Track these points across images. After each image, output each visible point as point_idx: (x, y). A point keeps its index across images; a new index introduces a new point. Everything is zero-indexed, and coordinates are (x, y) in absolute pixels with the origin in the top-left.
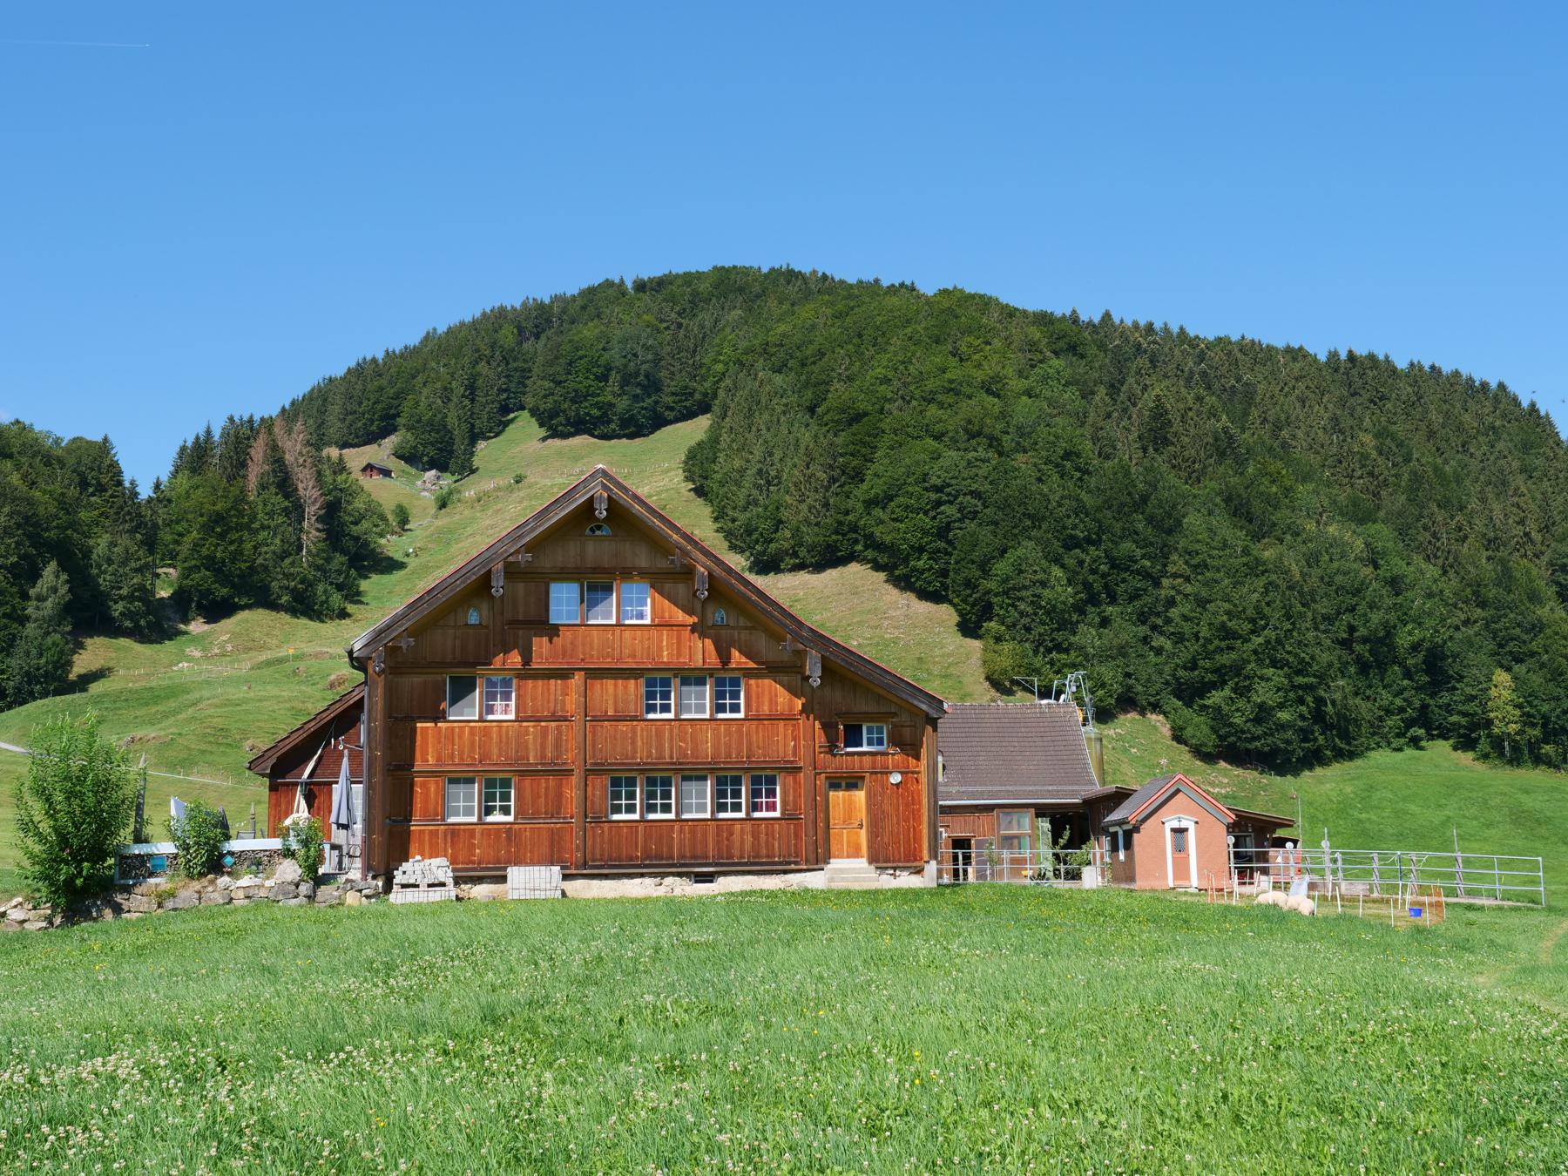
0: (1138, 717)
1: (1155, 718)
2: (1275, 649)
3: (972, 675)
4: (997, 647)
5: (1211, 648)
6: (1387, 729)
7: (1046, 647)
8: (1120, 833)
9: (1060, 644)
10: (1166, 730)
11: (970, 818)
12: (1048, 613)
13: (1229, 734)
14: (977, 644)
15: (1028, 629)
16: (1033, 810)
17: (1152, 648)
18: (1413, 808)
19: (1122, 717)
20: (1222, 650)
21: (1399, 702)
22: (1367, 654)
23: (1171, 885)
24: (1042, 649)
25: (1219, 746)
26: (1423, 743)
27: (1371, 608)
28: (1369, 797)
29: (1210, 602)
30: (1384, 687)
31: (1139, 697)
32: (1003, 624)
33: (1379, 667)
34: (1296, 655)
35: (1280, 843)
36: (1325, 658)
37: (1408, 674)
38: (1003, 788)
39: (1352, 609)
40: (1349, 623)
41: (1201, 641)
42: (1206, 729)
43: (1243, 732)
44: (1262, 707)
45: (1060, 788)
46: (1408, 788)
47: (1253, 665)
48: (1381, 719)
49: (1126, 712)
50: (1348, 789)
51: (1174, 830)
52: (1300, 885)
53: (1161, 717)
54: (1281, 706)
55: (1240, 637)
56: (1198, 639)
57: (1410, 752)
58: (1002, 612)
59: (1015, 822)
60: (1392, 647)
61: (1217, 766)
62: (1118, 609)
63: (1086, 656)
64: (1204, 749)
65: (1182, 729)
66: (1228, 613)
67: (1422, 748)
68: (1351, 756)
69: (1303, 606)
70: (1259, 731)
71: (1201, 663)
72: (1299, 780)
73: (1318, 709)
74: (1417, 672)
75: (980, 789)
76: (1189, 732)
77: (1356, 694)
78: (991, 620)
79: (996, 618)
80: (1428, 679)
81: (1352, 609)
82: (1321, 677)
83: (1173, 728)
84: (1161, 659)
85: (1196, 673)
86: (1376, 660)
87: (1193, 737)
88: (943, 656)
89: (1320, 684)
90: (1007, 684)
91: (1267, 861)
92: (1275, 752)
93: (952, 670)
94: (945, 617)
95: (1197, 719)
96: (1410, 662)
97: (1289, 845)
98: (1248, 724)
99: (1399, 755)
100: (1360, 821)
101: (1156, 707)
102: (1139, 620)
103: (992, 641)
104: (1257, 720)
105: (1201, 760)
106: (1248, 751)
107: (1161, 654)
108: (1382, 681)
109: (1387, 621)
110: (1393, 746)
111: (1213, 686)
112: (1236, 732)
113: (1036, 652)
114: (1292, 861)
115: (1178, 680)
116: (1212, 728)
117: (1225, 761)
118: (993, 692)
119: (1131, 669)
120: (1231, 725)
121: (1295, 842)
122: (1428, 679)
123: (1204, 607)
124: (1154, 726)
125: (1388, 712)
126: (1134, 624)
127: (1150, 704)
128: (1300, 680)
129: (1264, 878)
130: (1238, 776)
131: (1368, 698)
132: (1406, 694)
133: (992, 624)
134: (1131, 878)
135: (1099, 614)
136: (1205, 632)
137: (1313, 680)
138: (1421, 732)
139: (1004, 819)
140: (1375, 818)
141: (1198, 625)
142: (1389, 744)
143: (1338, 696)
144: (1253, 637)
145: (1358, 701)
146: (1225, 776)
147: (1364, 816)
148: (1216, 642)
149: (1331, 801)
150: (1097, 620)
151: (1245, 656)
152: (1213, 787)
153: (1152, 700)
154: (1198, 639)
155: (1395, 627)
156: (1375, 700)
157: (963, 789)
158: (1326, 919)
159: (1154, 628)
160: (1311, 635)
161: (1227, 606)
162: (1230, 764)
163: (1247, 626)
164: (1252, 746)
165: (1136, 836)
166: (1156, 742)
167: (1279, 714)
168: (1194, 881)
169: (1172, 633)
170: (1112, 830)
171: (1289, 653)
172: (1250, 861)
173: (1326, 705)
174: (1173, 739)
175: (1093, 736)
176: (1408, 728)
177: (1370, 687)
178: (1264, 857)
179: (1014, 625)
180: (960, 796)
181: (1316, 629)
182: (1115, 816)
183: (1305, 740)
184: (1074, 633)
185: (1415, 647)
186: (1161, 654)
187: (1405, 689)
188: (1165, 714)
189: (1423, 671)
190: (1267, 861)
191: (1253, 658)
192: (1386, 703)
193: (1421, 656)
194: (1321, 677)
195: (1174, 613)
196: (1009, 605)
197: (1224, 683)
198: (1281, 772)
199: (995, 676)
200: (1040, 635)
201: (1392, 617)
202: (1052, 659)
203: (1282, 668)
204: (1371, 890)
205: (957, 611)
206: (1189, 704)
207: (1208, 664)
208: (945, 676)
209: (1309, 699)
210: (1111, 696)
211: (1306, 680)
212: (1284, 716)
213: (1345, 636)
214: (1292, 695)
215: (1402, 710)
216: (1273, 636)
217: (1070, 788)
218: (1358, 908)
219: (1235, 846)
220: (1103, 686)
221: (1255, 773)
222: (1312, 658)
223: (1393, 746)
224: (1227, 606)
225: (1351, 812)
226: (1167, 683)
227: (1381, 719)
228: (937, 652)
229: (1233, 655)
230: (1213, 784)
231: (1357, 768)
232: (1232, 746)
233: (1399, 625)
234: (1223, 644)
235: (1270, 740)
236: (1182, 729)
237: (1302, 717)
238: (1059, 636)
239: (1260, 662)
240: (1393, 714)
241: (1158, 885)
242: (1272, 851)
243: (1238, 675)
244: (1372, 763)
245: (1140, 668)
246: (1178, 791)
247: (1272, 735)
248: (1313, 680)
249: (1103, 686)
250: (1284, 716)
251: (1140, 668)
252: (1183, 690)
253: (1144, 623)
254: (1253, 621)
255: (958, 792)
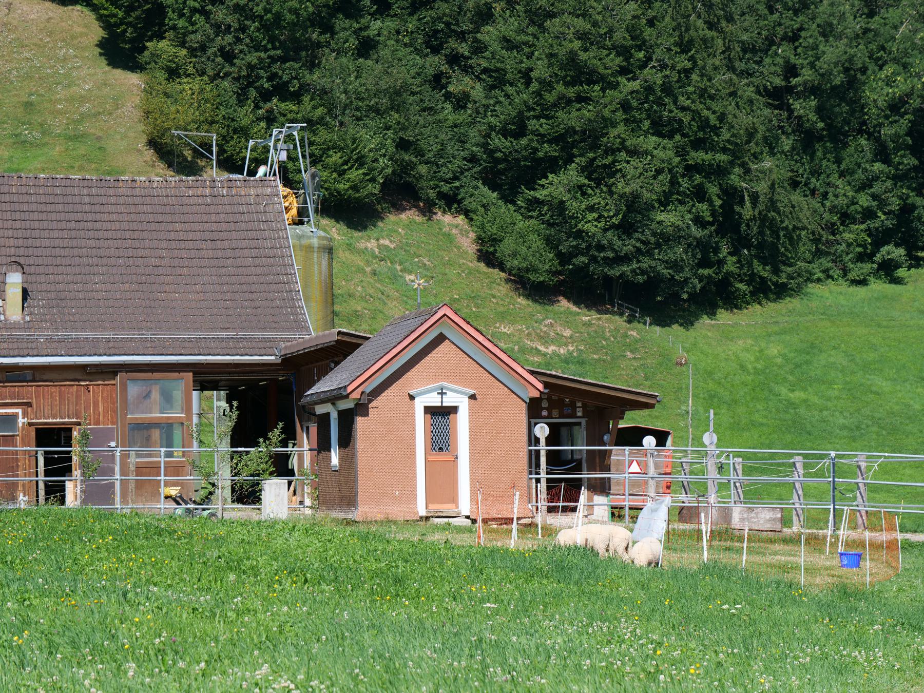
0: (419, 219)
1: (447, 220)
2: (660, 102)
3: (124, 137)
4: (172, 87)
5: (550, 97)
6: (843, 247)
7: (259, 89)
8: (334, 416)
9: (287, 84)
10: (468, 244)
11: (72, 390)
12: (265, 27)
13: (576, 252)
14: (133, 80)
15: (228, 56)
16: (190, 375)
17: (448, 96)
18: (880, 383)
19: (391, 218)
20: (569, 102)
21: (864, 200)
22: (813, 117)
23: (422, 512)
24: (253, 93)
25: (556, 273)
26: (901, 272)
27: (824, 35)
28: (808, 363)
29: (552, 15)
30: (842, 175)
31: (423, 183)
32: (183, 44)
33: (834, 139)
34: (696, 113)
35: (633, 437)
36: (744, 120)
37: (882, 154)
38: (136, 334)
39: (793, 38)
40: (787, 62)
41: (535, 86)
42: (537, 243)
43: (600, 248)
44: (633, 203)
45: (242, 335)
46: (874, 348)
47: (621, 128)
48: (832, 228)
49: (399, 208)
50: (773, 350)
51: (430, 411)
52: (654, 511)
53: (460, 220)
54: (664, 202)
55: (602, 79)
56: (528, 82)
57: (878, 286)
58: (181, 23)
59: (156, 395)
60: (857, 106)
61: (556, 307)
62: (390, 24)
63: (331, 108)
64: (532, 277)
65: (495, 241)
66: (582, 36)
67: (898, 281)
68: (781, 292)
69: (711, 26)
70: (628, 246)
71: (532, 124)
72: (692, 333)
73: (728, 208)
74: (897, 149)
75: (91, 334)
76: (507, 246)
77: (795, 184)
78: (161, 37)
79: (170, 34)
80: (914, 162)
81: (793, 38)
82: (736, 153)
83: (480, 240)
84: (462, 117)
85: (524, 141)
86: (829, 127)
87: (514, 255)
88: (71, 100)
89: (732, 163)
90: (188, 154)
91: (607, 469)
92: (654, 282)
93: (87, 127)
94: (78, 30)
95: (521, 224)
96: (887, 131)
97: (649, 441)
98: (609, 234)
99: (861, 292)
100: (791, 404)
101: (451, 202)
102: (427, 44)
103: (161, 76)
104: (626, 228)
105: (527, 296)
106: (608, 280)
107: (464, 107)
108: (838, 161)
109: (851, 60)
110: (851, 276)
111: (553, 165)
112: (589, 247)
113: (241, 98)
114: (652, 471)
115: (491, 153)
116: (548, 240)
117: (569, 299)
118: (161, 167)
119: (409, 135)
120: (579, 234)
121: (661, 438)
122: (914, 162)
123: (541, 26)
124: (448, 236)
125: (846, 217)
126: (418, 51)
127: (441, 195)
128: (700, 156)
129: (599, 499)
130: (589, 324)
131: (813, 192)
132: (877, 188)
133: (163, 44)
134: (349, 500)
135: (357, 32)
136: (541, 70)
137: (722, 157)
138: (899, 253)
139: (134, 390)
140: (815, 399)
141: (530, 56)
142: (845, 272)
143: (762, 187)
144: (622, 80)
145: (796, 197)
146: (567, 324)
147: (799, 395)
148: (560, 88)
149: (743, 367)
150: (353, 42)
151: (606, 113)
152: (546, 343)
153: (446, 188)
154: (528, 82)
155: (864, 70)
156: (825, 195)
157: (61, 335)
158: (676, 573)
159: (454, 59)
160: (721, 78)
161: (581, 24)
162: (577, 303)
163: (615, 61)
164: (615, 272)
165: (360, 421)
166: (450, 264)
167: (660, 217)
168: (465, 506)
169: (485, 71)
170: (320, 410)
171: (683, 109)
172: (578, 468)
173: (742, 202)
174: (479, 259)
175: (315, 242)
176: (878, 244)
177: (816, 173)
178: (601, 461)
179: (203, 48)
180: (53, 347)
181: (731, 68)
182: (324, 386)
183: (704, 263)
184: (313, 65)
185: (896, 107)
186: (464, 107)
187: (876, 178)
188: (467, 213)
189: (908, 147)
190: (607, 469)
191: (620, 115)
192: (842, 201)
193: (904, 123)
194: (736, 153)
195: (489, 34)
196: (194, 11)
197: (570, 160)
198: (663, 320)
199: (166, 140)
200: (251, 67)
201: (860, 53)
202: (270, 111)
203: (671, 137)
204: (786, 521)
205: (100, 18)
206: (509, 198)
207: (544, 126)
208: (75, 138)
209: (713, 190)
210: (373, 180)
211: (708, 157)
212: (668, 218)
213: (778, 81)
214: (685, 183)
215: (869, 214)
216: (658, 79)
217: (260, 335)
218: (740, 551)
219: (550, 441)
220: (360, 161)
221: (619, 322)
222: (722, 118)
223: (851, 276)
224: (581, 24)
225: (777, 388)
226: (473, 159)
227: (832, 228)
228: (61, 93)
229: (588, 112)
230: (544, 339)
231: (790, 312)
232: (582, 271)
233: (872, 67)
234: (571, 92)
235: (646, 262)
236: (495, 241)
237: (699, 221)
238: (287, 69)
239: (633, 124)
240: (854, 221)
241: (398, 512)
242: (620, 454)
243: (594, 147)
244: (814, 304)
245: (426, 131)
246: (441, 339)
247: (649, 253)
248: (722, 157)
249: (360, 161)
250: (668, 218)
251: (426, 131)
252: (502, 172)
253: (436, 50)
254: (624, 52)
255: (50, 340)
